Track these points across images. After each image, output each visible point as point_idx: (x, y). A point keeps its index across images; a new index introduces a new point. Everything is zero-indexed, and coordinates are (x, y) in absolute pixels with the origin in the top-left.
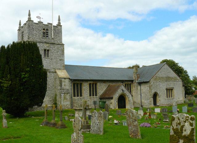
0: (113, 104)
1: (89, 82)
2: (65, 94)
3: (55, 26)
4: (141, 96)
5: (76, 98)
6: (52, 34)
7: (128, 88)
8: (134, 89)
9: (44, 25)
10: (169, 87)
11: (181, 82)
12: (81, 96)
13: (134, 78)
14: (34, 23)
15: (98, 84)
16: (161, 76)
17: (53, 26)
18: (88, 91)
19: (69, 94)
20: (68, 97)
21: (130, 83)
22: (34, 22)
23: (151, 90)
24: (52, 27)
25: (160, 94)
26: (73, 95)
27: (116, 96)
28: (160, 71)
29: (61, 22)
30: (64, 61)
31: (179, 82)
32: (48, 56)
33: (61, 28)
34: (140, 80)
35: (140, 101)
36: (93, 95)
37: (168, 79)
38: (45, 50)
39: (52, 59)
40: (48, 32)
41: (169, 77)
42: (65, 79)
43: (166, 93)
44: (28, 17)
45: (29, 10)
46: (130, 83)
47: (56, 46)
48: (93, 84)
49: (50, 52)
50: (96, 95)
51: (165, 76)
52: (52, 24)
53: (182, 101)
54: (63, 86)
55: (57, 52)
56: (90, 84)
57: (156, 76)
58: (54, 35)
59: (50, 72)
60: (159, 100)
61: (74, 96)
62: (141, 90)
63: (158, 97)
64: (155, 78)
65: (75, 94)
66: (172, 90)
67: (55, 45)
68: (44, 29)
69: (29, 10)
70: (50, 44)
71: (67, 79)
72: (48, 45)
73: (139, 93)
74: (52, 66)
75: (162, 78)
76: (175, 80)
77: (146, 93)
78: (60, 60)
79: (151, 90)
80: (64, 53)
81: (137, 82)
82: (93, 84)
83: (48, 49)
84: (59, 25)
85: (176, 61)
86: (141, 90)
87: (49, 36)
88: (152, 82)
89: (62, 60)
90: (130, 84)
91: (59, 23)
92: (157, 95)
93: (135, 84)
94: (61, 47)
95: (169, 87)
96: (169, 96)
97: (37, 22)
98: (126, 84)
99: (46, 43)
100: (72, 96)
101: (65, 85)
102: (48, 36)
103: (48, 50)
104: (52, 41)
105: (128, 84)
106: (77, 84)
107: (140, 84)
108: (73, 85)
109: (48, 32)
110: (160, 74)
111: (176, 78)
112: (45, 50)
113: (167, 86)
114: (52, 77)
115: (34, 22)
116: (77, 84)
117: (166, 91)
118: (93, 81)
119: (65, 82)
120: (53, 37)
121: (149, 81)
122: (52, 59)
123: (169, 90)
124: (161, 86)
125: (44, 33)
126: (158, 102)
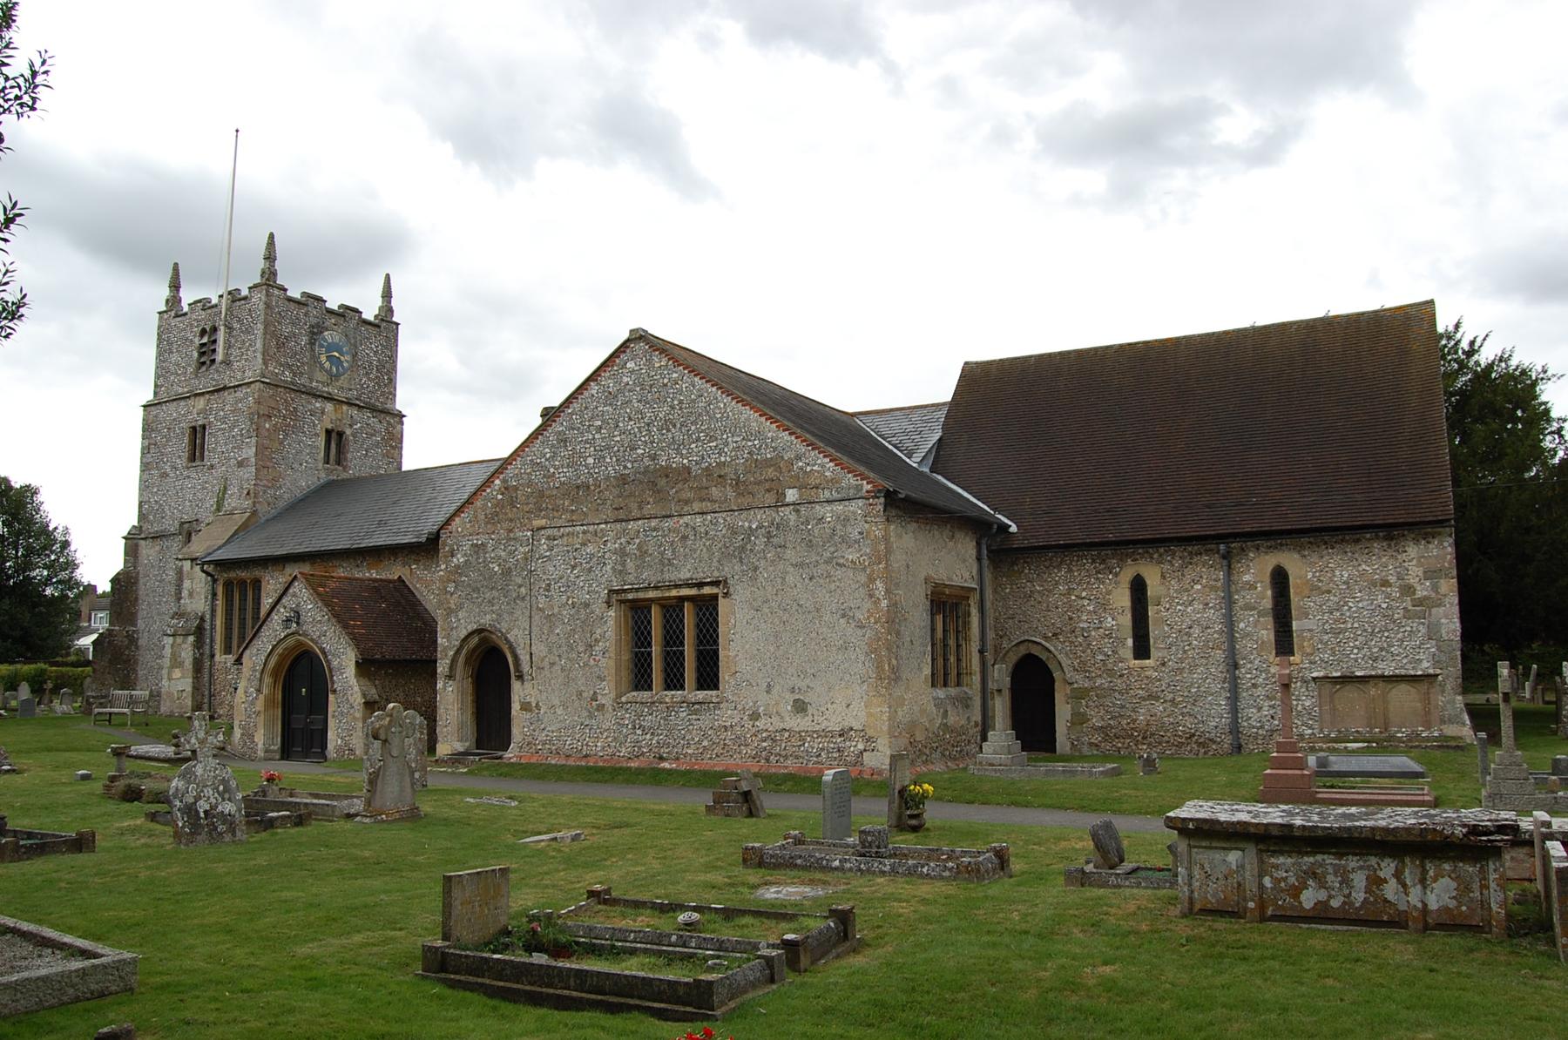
10: (649, 576)
16: (564, 475)
29: (279, 266)
41: (666, 472)
72: (201, 403)
103: (204, 427)
108: (220, 590)
111: (771, 473)
123: (672, 609)
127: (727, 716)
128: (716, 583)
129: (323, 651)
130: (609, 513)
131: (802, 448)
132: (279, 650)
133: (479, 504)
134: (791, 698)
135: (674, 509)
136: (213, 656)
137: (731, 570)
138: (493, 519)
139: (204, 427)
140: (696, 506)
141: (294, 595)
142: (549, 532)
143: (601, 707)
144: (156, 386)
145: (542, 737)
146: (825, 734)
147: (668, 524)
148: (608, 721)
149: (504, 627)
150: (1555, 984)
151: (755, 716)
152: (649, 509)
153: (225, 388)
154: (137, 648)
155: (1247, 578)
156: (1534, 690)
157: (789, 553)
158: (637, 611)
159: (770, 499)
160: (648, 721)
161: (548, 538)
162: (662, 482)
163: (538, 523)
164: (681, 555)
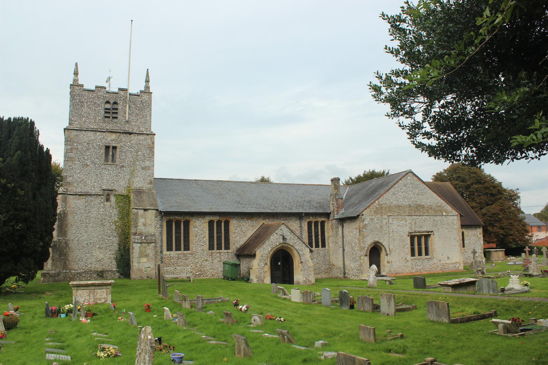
0: (259, 267)
1: (208, 219)
4: (344, 250)
5: (174, 253)
6: (125, 112)
10: (418, 229)
11: (455, 218)
12: (187, 248)
13: (332, 208)
15: (234, 224)
16: (395, 203)
17: (130, 95)
18: (204, 237)
19: (153, 245)
21: (320, 219)
22: (84, 87)
23: (364, 237)
24: (126, 97)
25: (391, 247)
27: (265, 251)
29: (150, 84)
32: (113, 160)
34: (342, 213)
37: (418, 209)
38: (107, 148)
41: (420, 205)
44: (144, 84)
46: (323, 219)
49: (118, 150)
50: (227, 247)
51: (406, 202)
52: (126, 90)
53: (457, 265)
56: (211, 223)
57: (379, 204)
61: (169, 249)
62: (343, 237)
63: (383, 254)
65: (180, 242)
66: (427, 237)
68: (108, 102)
70: (118, 134)
72: (114, 136)
73: (340, 243)
77: (353, 245)
80: (153, 152)
81: (336, 217)
82: (220, 224)
84: (147, 91)
86: (343, 237)
87: (119, 117)
88: (367, 216)
89: (150, 168)
90: (323, 223)
91: (147, 87)
92: (381, 249)
102: (116, 118)
103: (115, 148)
104: (127, 128)
105: (316, 223)
106: (177, 225)
107: (342, 221)
108: (165, 224)
109: (117, 109)
111: (440, 208)
112: (107, 148)
115: (84, 87)
116: (177, 225)
118: (220, 216)
120: (127, 119)
121: (358, 216)
123: (419, 237)
125: (107, 111)
126: (384, 266)
127: (435, 261)
128: (431, 232)
129: (272, 250)
131: (446, 204)
132: (274, 249)
133: (371, 207)
136: (161, 252)
141: (281, 230)
143: (408, 261)
144: (70, 120)
147: (420, 217)
148: (409, 264)
149: (381, 241)
150: (278, 330)
151: (440, 261)
152: (417, 214)
154: (69, 248)
156: (53, 265)
158: (412, 238)
160: (419, 263)
163: (389, 214)
164: (423, 225)
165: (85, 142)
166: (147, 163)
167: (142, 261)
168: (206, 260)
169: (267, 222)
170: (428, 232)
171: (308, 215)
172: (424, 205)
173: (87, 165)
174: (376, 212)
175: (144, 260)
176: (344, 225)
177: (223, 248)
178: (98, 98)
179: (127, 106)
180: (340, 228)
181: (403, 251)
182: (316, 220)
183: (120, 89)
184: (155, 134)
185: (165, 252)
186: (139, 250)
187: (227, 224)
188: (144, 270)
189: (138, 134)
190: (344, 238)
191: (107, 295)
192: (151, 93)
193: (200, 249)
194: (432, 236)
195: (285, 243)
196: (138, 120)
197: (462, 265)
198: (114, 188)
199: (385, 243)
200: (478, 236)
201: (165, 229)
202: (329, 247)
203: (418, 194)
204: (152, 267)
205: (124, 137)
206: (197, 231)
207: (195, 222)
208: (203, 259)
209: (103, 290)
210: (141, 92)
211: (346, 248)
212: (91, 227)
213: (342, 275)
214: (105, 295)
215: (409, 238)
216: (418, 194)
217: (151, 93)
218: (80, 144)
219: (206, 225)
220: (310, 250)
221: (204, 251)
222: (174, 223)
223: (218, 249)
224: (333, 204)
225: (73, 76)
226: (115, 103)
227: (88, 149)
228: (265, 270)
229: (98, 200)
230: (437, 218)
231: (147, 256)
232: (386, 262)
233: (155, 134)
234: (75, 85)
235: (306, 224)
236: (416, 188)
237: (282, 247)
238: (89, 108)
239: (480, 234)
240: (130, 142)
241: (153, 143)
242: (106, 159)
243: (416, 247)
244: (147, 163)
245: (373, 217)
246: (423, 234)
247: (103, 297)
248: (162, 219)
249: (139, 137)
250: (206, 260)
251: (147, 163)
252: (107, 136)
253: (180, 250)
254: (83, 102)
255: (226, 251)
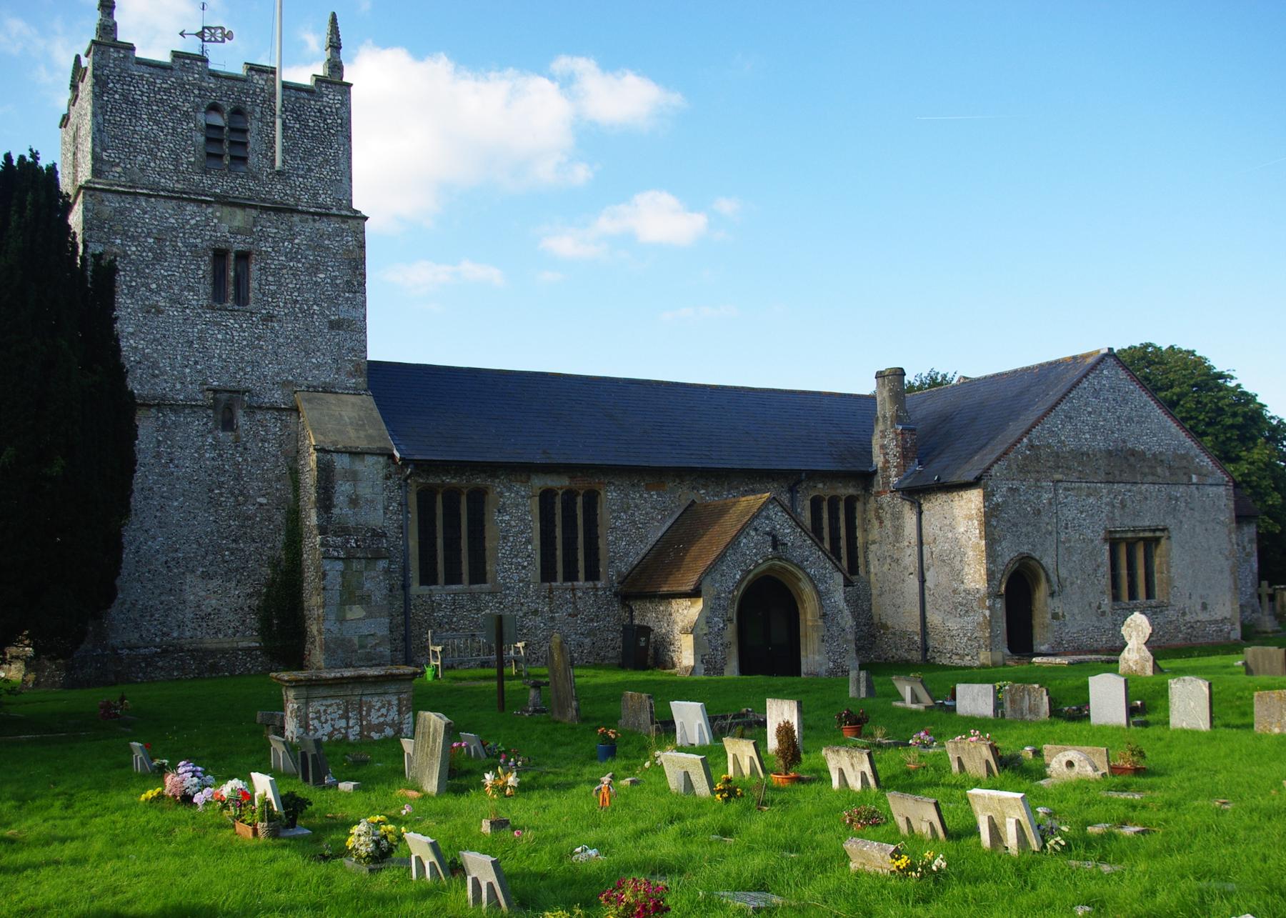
1: (540, 482)
2: (355, 565)
3: (299, 88)
5: (440, 592)
6: (275, 143)
7: (835, 540)
8: (875, 533)
9: (215, 75)
10: (1129, 522)
12: (478, 575)
14: (141, 62)
17: (286, 86)
18: (529, 541)
19: (382, 564)
20: (374, 581)
24: (273, 95)
26: (414, 573)
28: (1064, 406)
30: (363, 330)
31: (1211, 490)
32: (241, 298)
33: (346, 104)
35: (917, 619)
36: (571, 575)
37: (1125, 463)
38: (220, 255)
39: (270, 317)
40: (245, 131)
41: (1133, 453)
42: (355, 454)
43: (1106, 568)
45: (334, 15)
46: (851, 491)
47: (305, 229)
48: (570, 495)
49: (254, 268)
50: (592, 574)
51: (1100, 444)
52: (273, 71)
53: (1227, 628)
54: (341, 509)
55: (314, 269)
56: (546, 498)
57: (1031, 447)
58: (285, 151)
59: (251, 410)
60: (1055, 616)
61: (428, 577)
62: (921, 543)
63: (1041, 593)
64: (1026, 458)
66: (1151, 543)
67: (296, 218)
68: (214, 108)
69: (334, 15)
70: (254, 213)
71: (370, 460)
72: (239, 218)
74: (270, 370)
75: (1080, 455)
76: (1176, 471)
78: (335, 325)
79: (1210, 871)
83: (238, 245)
85: (1219, 364)
86: (921, 543)
87: (253, 160)
89: (354, 328)
90: (851, 502)
91: (335, 66)
92: (1036, 579)
93: (886, 498)
94: (339, 233)
95: (1124, 522)
96: (1133, 595)
97: (167, 59)
98: (816, 504)
99: (224, 201)
100: (405, 570)
101: (354, 502)
103: (243, 257)
104: (278, 192)
105: (833, 502)
108: (413, 499)
110: (1064, 433)
111: (1184, 463)
112: (220, 255)
113: (1112, 519)
114: (271, 447)
115: (139, 54)
117: (1107, 554)
119: (353, 476)
120: (278, 164)
122: (270, 317)
123: (1131, 545)
124: (1070, 514)
130: (1102, 476)
131: (1198, 451)
133: (1012, 455)
134: (1200, 601)
135: (1139, 478)
136: (405, 587)
137: (1170, 522)
138: (1023, 470)
139: (243, 257)
140: (1150, 478)
141: (767, 518)
142: (1065, 485)
143: (1103, 613)
145: (1067, 638)
146: (1216, 622)
149: (1037, 555)
151: (1184, 614)
153: (293, 211)
155: (962, 530)
157: (1196, 514)
158: (1114, 543)
159: (1185, 479)
161: (1066, 489)
162: (1132, 459)
163: (1058, 476)
164: (1145, 507)
165: (148, 235)
166: (344, 308)
167: (349, 616)
168: (535, 612)
169: (704, 495)
170: (1154, 531)
171: (814, 475)
172: (1144, 453)
173: (159, 311)
174: (1023, 470)
175: (356, 612)
176: (925, 507)
177: (581, 575)
178: (185, 92)
179: (278, 122)
180: (910, 519)
181: (1093, 583)
182: (833, 493)
183: (252, 68)
184: (366, 218)
185: (416, 588)
186: (340, 580)
187: (592, 500)
188: (356, 640)
189: (313, 214)
190: (925, 548)
191: (400, 712)
192: (349, 85)
193: (516, 577)
194: (1163, 541)
195: (780, 559)
196: (310, 170)
197: (1238, 627)
198: (243, 385)
199: (1048, 561)
200: (1244, 548)
201: (413, 516)
202: (868, 572)
203: (1130, 420)
204: (379, 634)
205: (272, 226)
206: (508, 523)
207: (501, 494)
208: (525, 608)
209: (388, 698)
210: (318, 80)
211: (929, 576)
212: (176, 509)
213: (916, 656)
214: (393, 715)
215: (1107, 547)
216: (1130, 420)
217: (349, 85)
218: (133, 238)
219: (534, 505)
220: (846, 578)
221: (528, 584)
222: (439, 498)
223: (566, 579)
224: (883, 447)
225: (98, 15)
226: (238, 112)
227: (159, 258)
228: (726, 640)
229: (196, 425)
230: (1180, 491)
231: (364, 600)
232: (1049, 616)
233: (366, 218)
234: (107, 40)
235: (808, 503)
236: (1125, 401)
237: (771, 568)
238: (157, 123)
239: (1250, 541)
240: (291, 241)
241: (362, 246)
242: (218, 294)
243: (1124, 572)
244: (344, 308)
245: (1016, 484)
246: (1141, 535)
247: (389, 719)
248: (403, 485)
249: (317, 225)
250: (535, 612)
251: (344, 312)
252: (220, 219)
253: (460, 582)
254: (134, 103)
255: (590, 584)
